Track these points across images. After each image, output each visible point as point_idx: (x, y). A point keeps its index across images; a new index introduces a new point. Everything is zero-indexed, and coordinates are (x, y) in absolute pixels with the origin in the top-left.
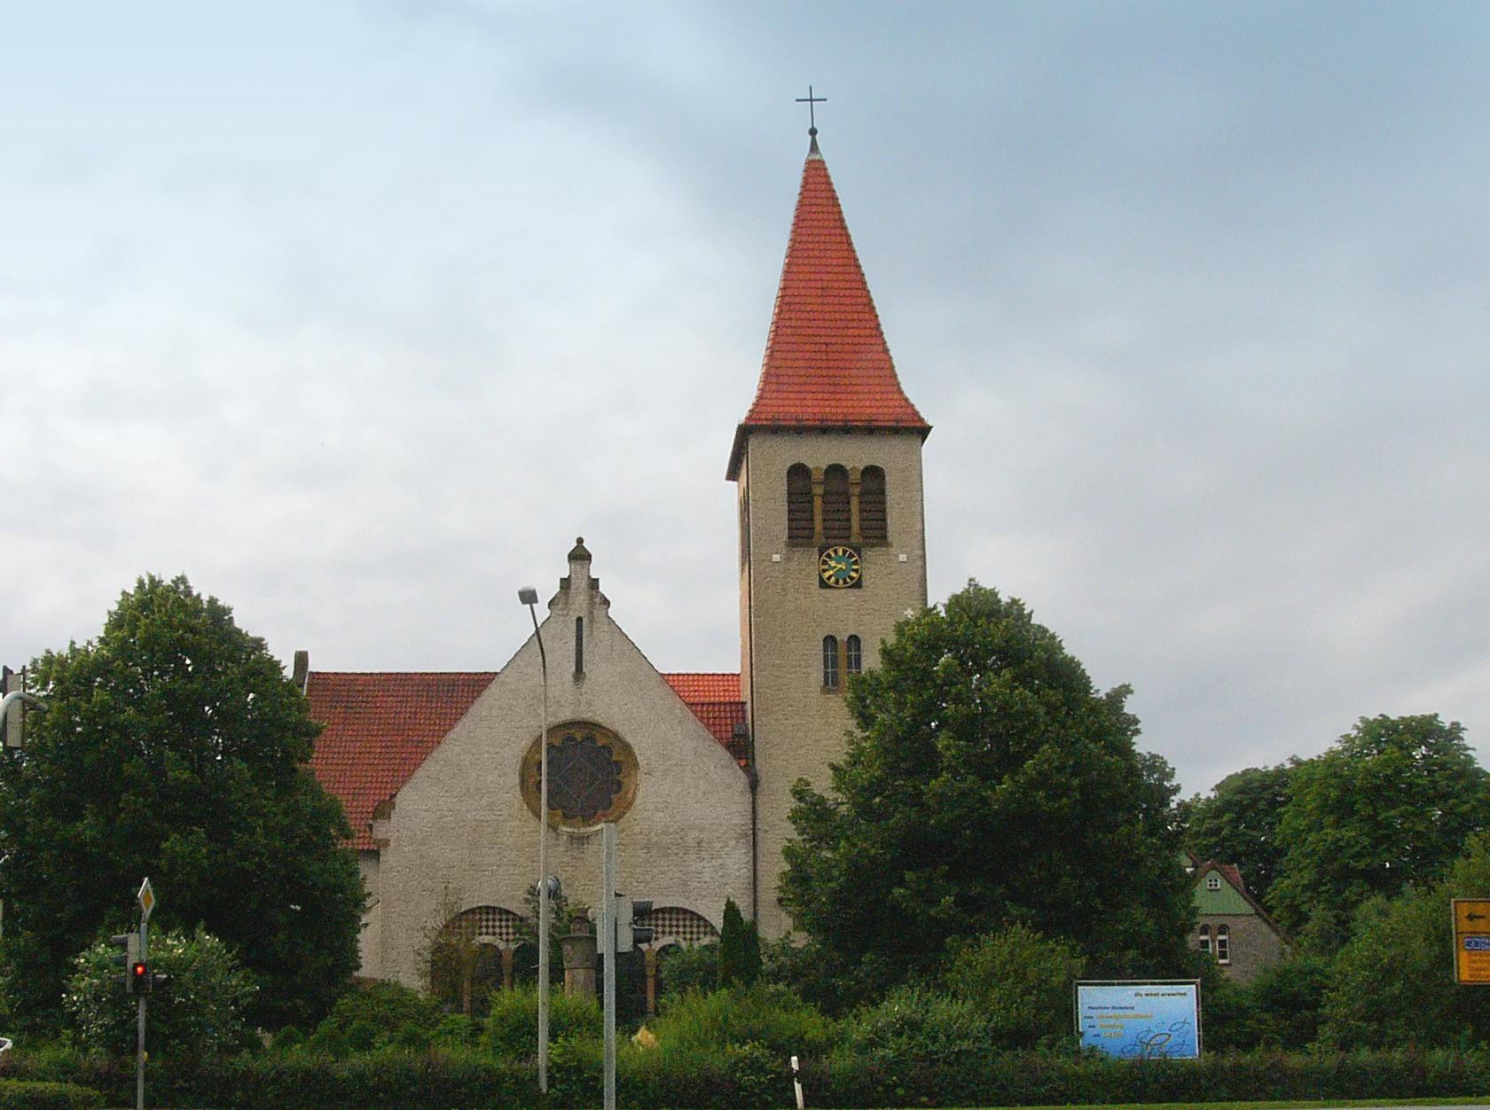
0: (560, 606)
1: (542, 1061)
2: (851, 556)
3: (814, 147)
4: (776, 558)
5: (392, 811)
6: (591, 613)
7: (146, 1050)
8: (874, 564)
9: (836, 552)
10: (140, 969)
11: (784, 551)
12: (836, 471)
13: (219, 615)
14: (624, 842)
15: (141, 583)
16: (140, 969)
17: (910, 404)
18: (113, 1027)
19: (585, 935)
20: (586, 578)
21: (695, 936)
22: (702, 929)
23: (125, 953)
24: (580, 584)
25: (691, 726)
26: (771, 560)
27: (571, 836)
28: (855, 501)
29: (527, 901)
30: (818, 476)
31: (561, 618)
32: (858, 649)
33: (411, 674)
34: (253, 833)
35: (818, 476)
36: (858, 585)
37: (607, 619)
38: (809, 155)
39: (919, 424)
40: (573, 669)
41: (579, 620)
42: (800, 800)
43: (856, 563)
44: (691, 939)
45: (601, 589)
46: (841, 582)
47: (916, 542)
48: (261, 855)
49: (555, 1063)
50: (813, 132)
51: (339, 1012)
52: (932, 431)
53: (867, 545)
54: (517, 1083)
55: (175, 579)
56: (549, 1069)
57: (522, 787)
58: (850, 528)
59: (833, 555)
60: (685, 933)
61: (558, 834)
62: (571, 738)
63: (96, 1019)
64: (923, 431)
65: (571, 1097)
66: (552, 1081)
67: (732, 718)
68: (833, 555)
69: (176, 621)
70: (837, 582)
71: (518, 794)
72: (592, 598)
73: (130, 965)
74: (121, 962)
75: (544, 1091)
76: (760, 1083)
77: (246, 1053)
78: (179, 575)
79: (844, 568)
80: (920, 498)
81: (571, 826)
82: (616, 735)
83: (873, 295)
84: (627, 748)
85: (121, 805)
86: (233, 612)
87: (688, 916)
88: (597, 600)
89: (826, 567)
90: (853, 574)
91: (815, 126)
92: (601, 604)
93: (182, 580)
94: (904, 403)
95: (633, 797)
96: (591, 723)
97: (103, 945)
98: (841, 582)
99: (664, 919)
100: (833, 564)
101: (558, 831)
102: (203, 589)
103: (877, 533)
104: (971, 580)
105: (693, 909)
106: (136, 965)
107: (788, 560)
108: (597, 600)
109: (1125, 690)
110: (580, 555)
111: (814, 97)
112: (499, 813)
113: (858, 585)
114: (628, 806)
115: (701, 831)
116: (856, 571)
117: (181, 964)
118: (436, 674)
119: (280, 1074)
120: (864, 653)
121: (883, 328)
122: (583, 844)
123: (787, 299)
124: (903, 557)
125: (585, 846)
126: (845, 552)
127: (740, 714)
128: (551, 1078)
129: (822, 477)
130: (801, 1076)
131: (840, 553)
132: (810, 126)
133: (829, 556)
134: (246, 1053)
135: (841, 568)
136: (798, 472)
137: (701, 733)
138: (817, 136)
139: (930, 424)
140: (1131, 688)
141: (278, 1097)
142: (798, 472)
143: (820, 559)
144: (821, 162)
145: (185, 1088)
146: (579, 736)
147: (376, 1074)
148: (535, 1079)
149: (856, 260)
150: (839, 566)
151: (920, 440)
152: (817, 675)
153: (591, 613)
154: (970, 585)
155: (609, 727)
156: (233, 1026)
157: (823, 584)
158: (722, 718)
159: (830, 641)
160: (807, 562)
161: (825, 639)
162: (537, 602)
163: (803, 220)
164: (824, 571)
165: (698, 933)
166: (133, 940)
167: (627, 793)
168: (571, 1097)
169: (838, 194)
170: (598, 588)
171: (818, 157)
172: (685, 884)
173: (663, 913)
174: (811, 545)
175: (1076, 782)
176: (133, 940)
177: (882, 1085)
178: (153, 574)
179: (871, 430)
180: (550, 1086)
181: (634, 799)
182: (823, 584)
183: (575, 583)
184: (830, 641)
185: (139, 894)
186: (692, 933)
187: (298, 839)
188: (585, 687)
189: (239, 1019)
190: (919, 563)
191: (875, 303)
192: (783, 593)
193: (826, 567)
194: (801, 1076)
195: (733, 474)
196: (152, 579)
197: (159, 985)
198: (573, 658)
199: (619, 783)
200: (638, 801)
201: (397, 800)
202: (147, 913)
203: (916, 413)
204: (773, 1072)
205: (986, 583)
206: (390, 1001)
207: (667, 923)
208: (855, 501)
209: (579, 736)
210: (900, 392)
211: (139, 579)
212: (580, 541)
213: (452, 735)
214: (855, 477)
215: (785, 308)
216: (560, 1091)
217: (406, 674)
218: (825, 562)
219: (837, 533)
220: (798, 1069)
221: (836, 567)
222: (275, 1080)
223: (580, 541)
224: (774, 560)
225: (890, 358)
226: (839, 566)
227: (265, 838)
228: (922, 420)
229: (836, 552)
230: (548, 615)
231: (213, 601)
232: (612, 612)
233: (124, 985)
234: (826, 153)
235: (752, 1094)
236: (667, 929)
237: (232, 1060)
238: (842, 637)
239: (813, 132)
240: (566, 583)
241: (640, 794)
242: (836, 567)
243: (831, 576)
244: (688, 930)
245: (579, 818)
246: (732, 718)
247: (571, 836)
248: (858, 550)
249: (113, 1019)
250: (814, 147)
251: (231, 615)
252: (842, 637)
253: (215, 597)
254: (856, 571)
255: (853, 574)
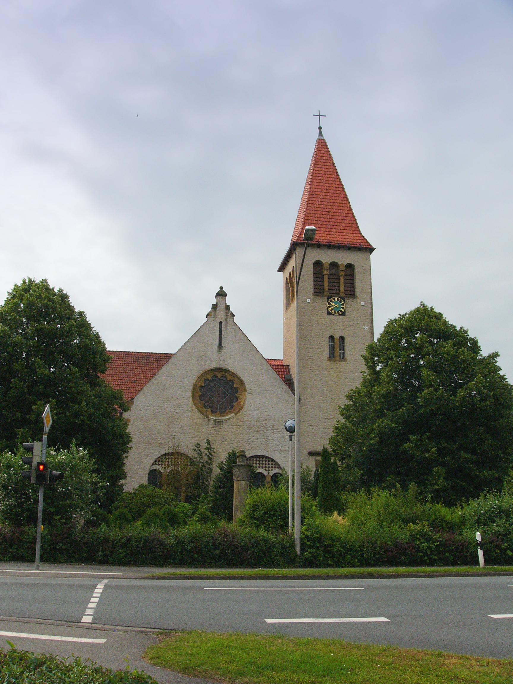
0: (213, 316)
1: (297, 535)
2: (341, 302)
3: (321, 134)
4: (308, 300)
5: (132, 406)
6: (226, 320)
7: (43, 524)
8: (351, 306)
9: (334, 299)
10: (41, 467)
11: (312, 298)
12: (334, 265)
13: (63, 297)
14: (239, 424)
15: (24, 282)
16: (41, 467)
17: (365, 238)
18: (15, 507)
19: (245, 464)
20: (224, 304)
21: (270, 469)
22: (274, 466)
23: (30, 455)
24: (221, 307)
25: (271, 373)
26: (306, 301)
27: (215, 421)
28: (342, 278)
29: (195, 450)
30: (326, 266)
31: (213, 321)
32: (343, 342)
33: (130, 352)
34: (80, 404)
35: (326, 266)
36: (344, 314)
37: (233, 323)
38: (318, 137)
39: (370, 247)
40: (218, 345)
41: (221, 323)
42: (351, 400)
43: (343, 304)
44: (269, 470)
45: (231, 310)
46: (336, 312)
47: (369, 298)
48: (84, 416)
49: (307, 536)
50: (320, 128)
51: (122, 500)
52: (375, 250)
53: (346, 297)
54: (282, 548)
55: (42, 280)
56: (301, 539)
57: (193, 398)
58: (339, 290)
59: (333, 301)
60: (266, 467)
61: (209, 420)
62: (216, 376)
63: (4, 501)
64: (371, 250)
65: (315, 557)
66: (303, 549)
67: (284, 372)
68: (333, 301)
69: (43, 296)
70: (335, 312)
71: (191, 400)
72: (227, 313)
73: (34, 464)
74: (29, 462)
75: (299, 553)
76: (429, 548)
77: (103, 526)
78: (44, 279)
79: (338, 306)
80: (370, 279)
81: (214, 416)
82: (236, 375)
83: (347, 194)
84: (241, 382)
85: (11, 385)
86: (69, 298)
87: (267, 460)
88: (229, 314)
89: (330, 305)
90: (342, 309)
91: (321, 126)
92: (230, 316)
93: (45, 281)
94: (363, 239)
95: (243, 404)
96: (225, 369)
97: (10, 453)
98: (336, 312)
99: (259, 461)
100: (333, 304)
101: (209, 418)
102: (55, 285)
103: (351, 293)
104: (422, 302)
105: (269, 456)
106: (39, 464)
107: (313, 301)
108: (229, 314)
109: (495, 355)
110: (221, 294)
111: (320, 115)
112: (182, 409)
113: (344, 314)
114: (242, 407)
115: (275, 420)
116: (343, 308)
117: (62, 467)
118: (141, 353)
119: (129, 540)
120: (346, 344)
121: (352, 207)
122: (220, 425)
123: (312, 193)
124: (363, 303)
125: (221, 426)
126: (338, 300)
127: (287, 370)
128: (302, 545)
129: (328, 267)
130: (482, 545)
131: (336, 300)
132: (319, 126)
133: (331, 301)
134: (103, 526)
135: (336, 307)
136: (318, 264)
137: (275, 376)
138: (322, 130)
139: (374, 246)
140: (499, 354)
141: (126, 556)
142: (318, 264)
143: (327, 302)
144: (324, 140)
145: (64, 549)
146: (219, 375)
147: (191, 542)
148: (293, 546)
149: (340, 179)
150: (336, 305)
151: (370, 253)
152: (326, 353)
153: (226, 320)
154: (421, 305)
155: (232, 371)
156: (93, 507)
157: (329, 313)
158: (282, 372)
159: (332, 338)
160: (322, 302)
161: (330, 337)
162: (213, 305)
163: (317, 162)
164: (329, 307)
165: (272, 467)
166: (37, 446)
167: (241, 402)
168: (315, 557)
169: (331, 153)
170: (229, 309)
171: (322, 138)
172: (267, 444)
173: (259, 458)
174: (324, 296)
175: (492, 393)
176: (37, 446)
177: (499, 549)
178: (31, 278)
179: (349, 248)
180: (303, 550)
181: (244, 403)
182: (329, 313)
183: (219, 306)
184: (332, 338)
185: (43, 416)
186: (269, 467)
187: (102, 410)
188: (223, 352)
189: (96, 503)
190: (370, 306)
191: (348, 197)
192: (311, 316)
193: (330, 305)
194: (482, 545)
195: (282, 269)
196: (30, 280)
197: (54, 479)
198: (218, 340)
199: (237, 398)
200: (246, 406)
201: (135, 401)
202: (47, 428)
203: (368, 243)
204: (437, 541)
205: (429, 305)
206: (149, 496)
207: (261, 462)
208: (342, 278)
209: (219, 375)
210: (361, 234)
211: (23, 279)
212: (221, 288)
213: (161, 372)
214: (342, 268)
215: (311, 196)
216: (310, 553)
217: (128, 352)
218: (330, 304)
219: (334, 292)
220: (481, 541)
221: (334, 306)
222: (124, 546)
223: (221, 288)
224: (307, 301)
225: (356, 220)
226: (336, 305)
227: (86, 407)
228: (371, 245)
229: (334, 299)
230: (206, 320)
231: (60, 291)
232: (236, 319)
233: (29, 477)
234: (325, 136)
235: (425, 555)
236: (261, 465)
237: (95, 531)
238: (337, 337)
239: (320, 128)
240: (214, 307)
241: (247, 403)
242: (334, 306)
243: (332, 309)
244: (267, 466)
245: (218, 413)
246: (284, 372)
247: (215, 421)
248: (344, 299)
249: (15, 501)
250: (321, 134)
251: (69, 299)
252: (337, 337)
253: (62, 289)
254: (335, 312)
255: (342, 309)
